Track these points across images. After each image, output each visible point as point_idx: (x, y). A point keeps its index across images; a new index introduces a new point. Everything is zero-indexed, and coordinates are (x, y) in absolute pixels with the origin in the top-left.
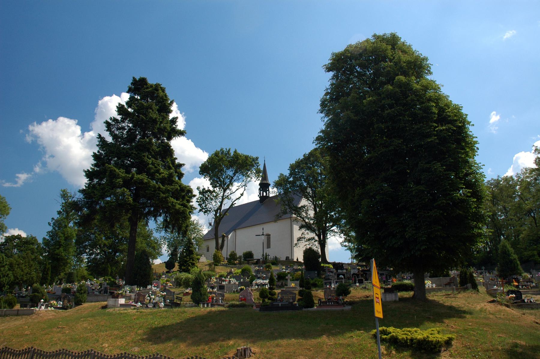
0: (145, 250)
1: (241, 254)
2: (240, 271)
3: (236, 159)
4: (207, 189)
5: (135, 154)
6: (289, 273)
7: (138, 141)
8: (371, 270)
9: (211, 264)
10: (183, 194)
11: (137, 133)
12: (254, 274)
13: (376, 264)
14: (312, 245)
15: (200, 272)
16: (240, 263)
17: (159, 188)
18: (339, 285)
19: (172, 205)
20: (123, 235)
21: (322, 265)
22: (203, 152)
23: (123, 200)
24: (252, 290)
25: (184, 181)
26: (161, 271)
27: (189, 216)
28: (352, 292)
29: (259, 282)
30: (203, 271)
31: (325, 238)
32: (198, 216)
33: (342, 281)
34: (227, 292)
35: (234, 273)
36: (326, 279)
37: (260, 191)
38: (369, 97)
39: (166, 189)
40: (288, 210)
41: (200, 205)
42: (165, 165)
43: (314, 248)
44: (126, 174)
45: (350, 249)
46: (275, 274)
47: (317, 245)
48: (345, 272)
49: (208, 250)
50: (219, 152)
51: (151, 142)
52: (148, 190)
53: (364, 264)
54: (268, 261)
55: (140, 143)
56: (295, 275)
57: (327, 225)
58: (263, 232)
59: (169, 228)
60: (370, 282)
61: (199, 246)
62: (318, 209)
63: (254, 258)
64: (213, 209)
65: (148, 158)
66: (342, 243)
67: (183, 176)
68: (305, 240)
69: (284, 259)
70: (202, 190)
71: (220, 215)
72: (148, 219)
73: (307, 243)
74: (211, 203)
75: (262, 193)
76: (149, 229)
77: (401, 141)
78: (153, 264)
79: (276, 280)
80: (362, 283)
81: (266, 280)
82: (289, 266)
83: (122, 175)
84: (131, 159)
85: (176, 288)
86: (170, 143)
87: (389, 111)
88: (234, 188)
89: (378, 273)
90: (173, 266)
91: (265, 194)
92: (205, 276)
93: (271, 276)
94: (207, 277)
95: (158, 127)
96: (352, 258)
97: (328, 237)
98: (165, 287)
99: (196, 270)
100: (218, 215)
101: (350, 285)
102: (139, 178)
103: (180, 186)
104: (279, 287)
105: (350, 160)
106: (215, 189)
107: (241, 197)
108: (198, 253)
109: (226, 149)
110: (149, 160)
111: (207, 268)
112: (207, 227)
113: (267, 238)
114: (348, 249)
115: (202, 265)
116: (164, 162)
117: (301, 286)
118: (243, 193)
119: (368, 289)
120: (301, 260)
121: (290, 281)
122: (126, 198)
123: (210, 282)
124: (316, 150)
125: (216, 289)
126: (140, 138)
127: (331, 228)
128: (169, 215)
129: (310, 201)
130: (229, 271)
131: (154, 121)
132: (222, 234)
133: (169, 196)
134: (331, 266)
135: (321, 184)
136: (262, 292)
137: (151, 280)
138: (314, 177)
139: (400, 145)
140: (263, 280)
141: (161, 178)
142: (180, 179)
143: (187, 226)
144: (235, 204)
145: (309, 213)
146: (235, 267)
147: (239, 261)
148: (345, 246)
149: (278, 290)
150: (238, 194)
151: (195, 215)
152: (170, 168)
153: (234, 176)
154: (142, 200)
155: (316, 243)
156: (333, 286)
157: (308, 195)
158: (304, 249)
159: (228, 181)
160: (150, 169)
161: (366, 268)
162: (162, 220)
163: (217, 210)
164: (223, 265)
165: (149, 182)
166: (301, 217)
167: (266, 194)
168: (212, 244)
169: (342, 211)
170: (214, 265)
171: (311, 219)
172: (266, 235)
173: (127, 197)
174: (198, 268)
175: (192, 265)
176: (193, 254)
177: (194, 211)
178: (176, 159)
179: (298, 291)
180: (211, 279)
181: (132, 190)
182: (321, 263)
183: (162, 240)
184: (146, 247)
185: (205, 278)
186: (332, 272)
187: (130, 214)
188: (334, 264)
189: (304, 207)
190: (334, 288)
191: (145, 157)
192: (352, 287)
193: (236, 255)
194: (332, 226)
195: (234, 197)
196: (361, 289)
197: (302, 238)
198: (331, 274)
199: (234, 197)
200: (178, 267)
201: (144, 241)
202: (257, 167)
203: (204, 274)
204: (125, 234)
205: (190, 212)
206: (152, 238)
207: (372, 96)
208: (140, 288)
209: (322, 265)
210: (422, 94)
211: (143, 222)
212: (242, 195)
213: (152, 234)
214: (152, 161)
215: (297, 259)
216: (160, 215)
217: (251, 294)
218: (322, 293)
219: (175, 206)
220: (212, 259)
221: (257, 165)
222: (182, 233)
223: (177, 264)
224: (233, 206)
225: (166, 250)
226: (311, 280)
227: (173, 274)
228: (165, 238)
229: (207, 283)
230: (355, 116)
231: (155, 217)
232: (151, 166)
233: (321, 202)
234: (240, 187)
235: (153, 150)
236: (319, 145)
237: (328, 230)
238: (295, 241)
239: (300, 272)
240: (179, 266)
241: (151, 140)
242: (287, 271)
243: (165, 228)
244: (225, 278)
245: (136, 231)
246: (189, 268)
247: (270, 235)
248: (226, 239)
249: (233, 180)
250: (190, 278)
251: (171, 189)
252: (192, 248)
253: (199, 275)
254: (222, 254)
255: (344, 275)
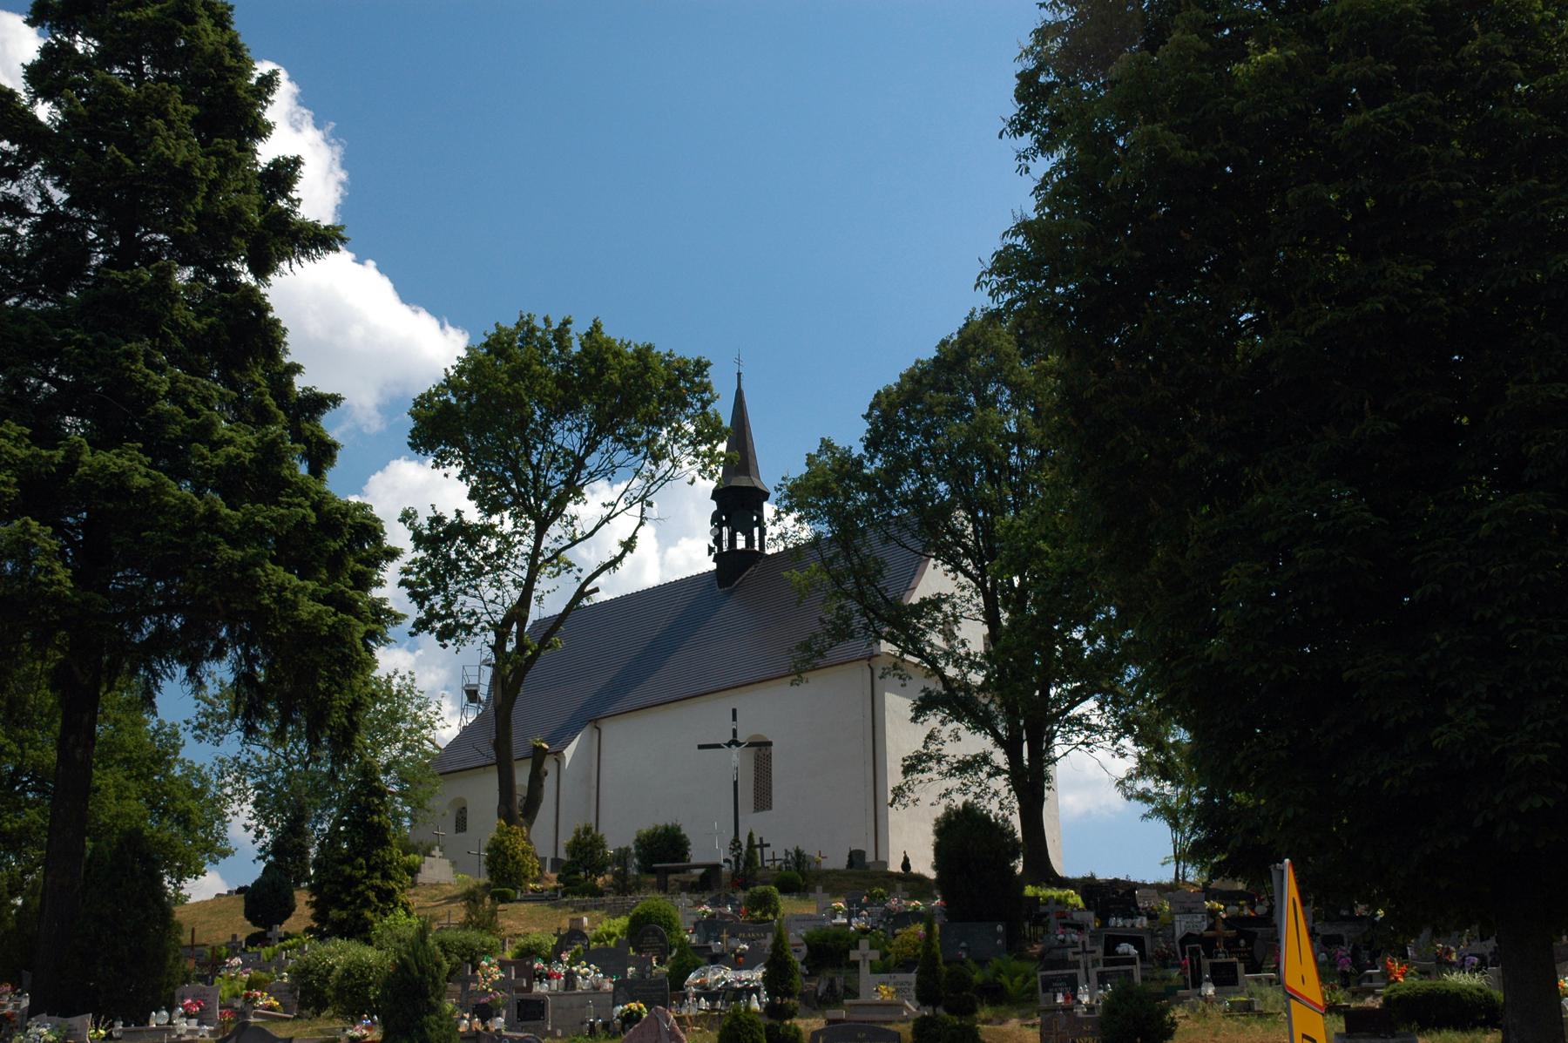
0: (139, 831)
1: (629, 842)
2: (620, 924)
3: (593, 370)
4: (450, 517)
5: (81, 344)
6: (864, 932)
7: (99, 282)
8: (1276, 918)
9: (479, 892)
10: (335, 545)
11: (92, 235)
12: (691, 938)
13: (1300, 882)
14: (977, 796)
15: (423, 933)
16: (623, 886)
17: (212, 515)
18: (1115, 995)
19: (280, 600)
20: (23, 755)
21: (1029, 890)
22: (442, 326)
23: (19, 576)
24: (680, 1020)
25: (338, 484)
26: (221, 934)
27: (364, 654)
28: (1179, 1029)
29: (718, 981)
30: (435, 926)
31: (1042, 758)
32: (411, 650)
33: (1129, 974)
34: (559, 1033)
35: (591, 934)
36: (1047, 961)
37: (720, 528)
38: (1264, 49)
39: (244, 524)
40: (858, 621)
41: (419, 597)
42: (241, 399)
43: (993, 807)
44: (34, 448)
45: (1168, 813)
46: (795, 936)
47: (1004, 793)
48: (1142, 930)
49: (461, 825)
50: (511, 334)
51: (167, 286)
52: (150, 528)
53: (1240, 886)
54: (759, 873)
55: (106, 288)
56: (894, 943)
57: (1053, 692)
58: (735, 732)
59: (265, 715)
60: (1270, 980)
61: (419, 805)
62: (1005, 616)
63: (693, 861)
64: (486, 617)
65: (150, 364)
66: (1129, 783)
67: (333, 457)
68: (945, 767)
69: (836, 860)
70: (426, 524)
71: (521, 647)
72: (155, 674)
73: (954, 782)
74: (476, 588)
75: (725, 536)
76: (161, 722)
77: (1425, 272)
78: (180, 900)
79: (800, 966)
80: (1233, 981)
81: (751, 967)
82: (864, 900)
83: (16, 451)
84: (60, 371)
85: (299, 1017)
86: (262, 290)
87: (1366, 115)
88: (586, 510)
89: (1312, 934)
90: (287, 909)
91: (741, 544)
92: (446, 951)
93: (779, 943)
94: (455, 958)
95: (200, 208)
96: (1177, 858)
97: (1058, 752)
98: (242, 1013)
99: (401, 923)
100: (510, 647)
101: (1171, 994)
102: (104, 467)
103: (316, 507)
104: (817, 1003)
105: (1165, 366)
106: (495, 519)
107: (622, 555)
108: (413, 841)
109: (546, 320)
110: (156, 378)
111: (459, 913)
112: (457, 708)
113: (757, 758)
114: (1156, 812)
115: (432, 898)
116: (232, 384)
117: (924, 997)
118: (633, 538)
119: (1261, 1015)
120: (924, 865)
121: (873, 971)
122: (39, 569)
123: (473, 985)
124: (993, 317)
125: (501, 1020)
126: (105, 263)
127: (1071, 707)
128: (264, 652)
129: (967, 574)
130: (566, 924)
131: (180, 179)
132: (532, 742)
133: (264, 557)
134: (1076, 899)
135: (1019, 493)
136: (730, 1027)
137: (169, 984)
138: (986, 454)
139: (1420, 291)
140: (737, 967)
141: (219, 467)
142: (317, 471)
143: (357, 706)
144: (596, 590)
145: (961, 635)
146: (596, 908)
147: (616, 875)
148: (1144, 797)
149: (810, 1016)
150: (608, 543)
151: (399, 647)
152: (263, 417)
153: (587, 454)
154: (122, 579)
155: (1000, 784)
156: (1085, 999)
157: (958, 544)
158: (940, 811)
159: (556, 479)
160: (161, 419)
161: (1253, 910)
162: (229, 678)
163: (507, 622)
164: (538, 897)
165: (159, 488)
166: (920, 653)
167: (750, 541)
168: (483, 794)
169: (1123, 622)
170: (493, 898)
171: (973, 665)
172: (751, 745)
173: (41, 561)
174: (409, 914)
175: (380, 900)
176: (385, 843)
177: (392, 632)
178: (295, 369)
179: (911, 1024)
180: (476, 967)
181: (70, 526)
182: (1020, 882)
183: (228, 779)
184: (143, 818)
185: (447, 966)
186: (1080, 928)
187: (60, 648)
188: (1090, 888)
189: (936, 603)
190: (1090, 1008)
191: (135, 361)
192: (1180, 1001)
193: (603, 846)
194: (1076, 697)
195: (587, 556)
196: (1228, 1014)
197: (930, 758)
198: (1075, 937)
199: (587, 556)
200: (309, 912)
201: (131, 784)
202: (704, 407)
203: (442, 944)
204: (31, 752)
205: (371, 635)
206: (177, 771)
207: (1277, 44)
208: (112, 1025)
209: (1029, 890)
210: (1543, 20)
211: (129, 687)
212: (629, 545)
213: (176, 749)
214: (174, 380)
215: (906, 860)
216: (218, 654)
217: (678, 1037)
218: (1030, 1031)
219: (294, 606)
220: (484, 868)
221: (701, 400)
222: (331, 739)
223: (302, 899)
224: (585, 602)
225: (247, 828)
226: (973, 966)
227: (284, 949)
228: (243, 768)
229: (458, 988)
230: (1188, 148)
231: (193, 661)
232: (166, 406)
233: (1022, 578)
234: (618, 509)
235: (175, 326)
236: (1008, 296)
237: (1054, 719)
238: (894, 777)
239: (920, 928)
240: (313, 905)
241: (165, 274)
242: (854, 921)
243: (246, 716)
244: (547, 961)
245: (92, 735)
246: (368, 914)
247: (770, 744)
248: (549, 765)
249: (584, 473)
250: (370, 967)
251: (273, 519)
252: (379, 813)
253: (415, 950)
254: (530, 843)
255: (1137, 942)
